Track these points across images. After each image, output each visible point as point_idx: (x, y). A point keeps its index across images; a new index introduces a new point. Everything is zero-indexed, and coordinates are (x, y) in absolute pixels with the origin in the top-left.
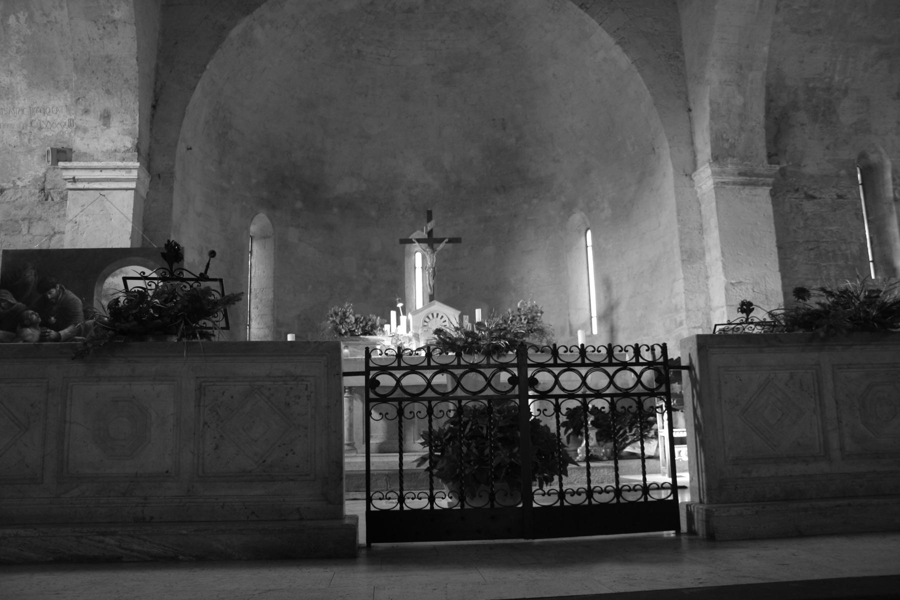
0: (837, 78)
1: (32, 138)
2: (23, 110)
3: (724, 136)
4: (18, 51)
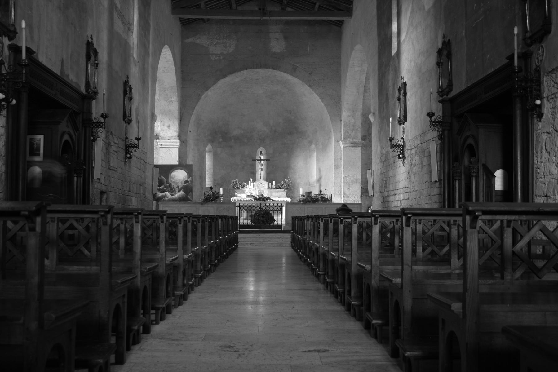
3: (348, 132)
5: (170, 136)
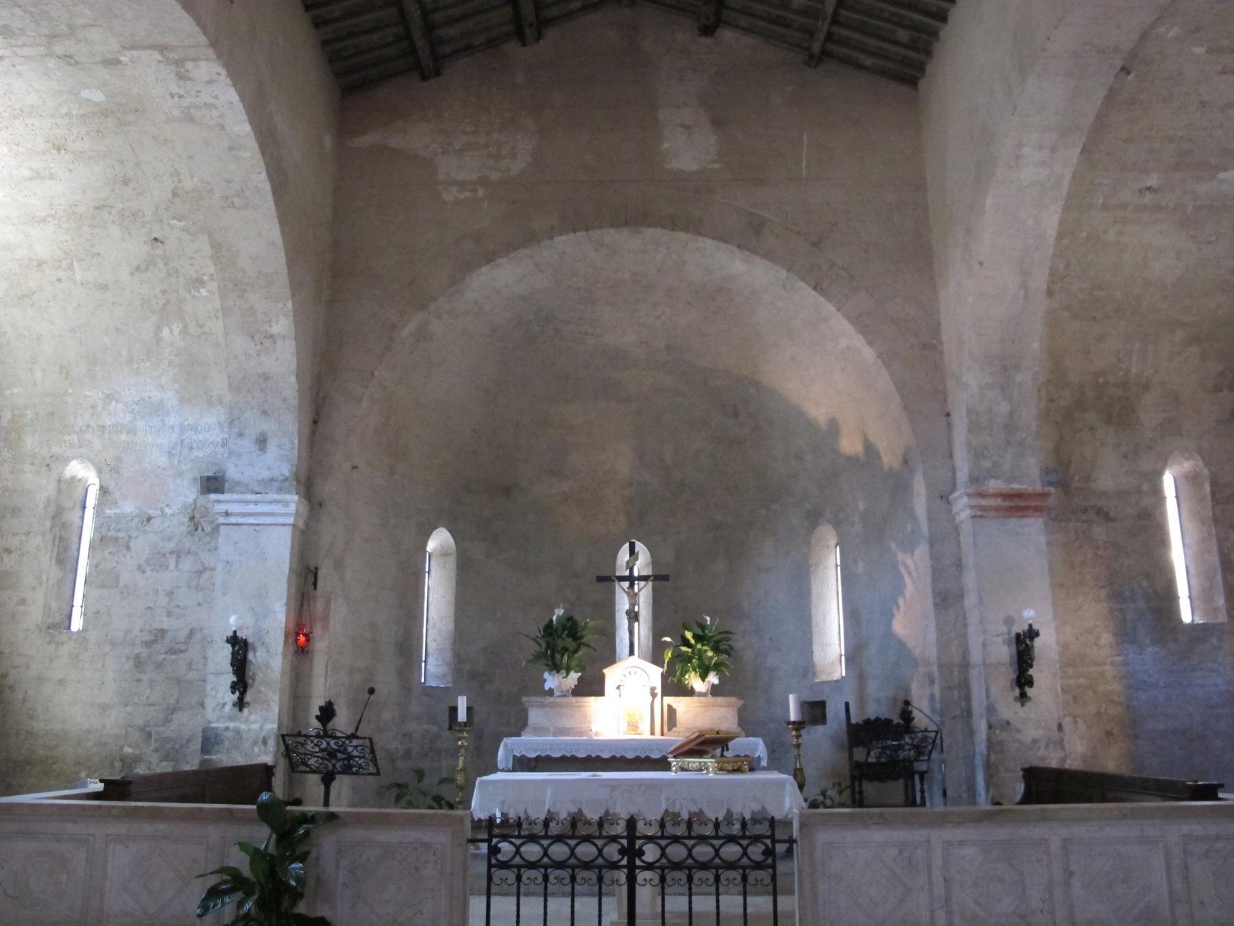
0: (1134, 371)
1: (182, 459)
2: (173, 428)
4: (170, 364)
5: (263, 480)
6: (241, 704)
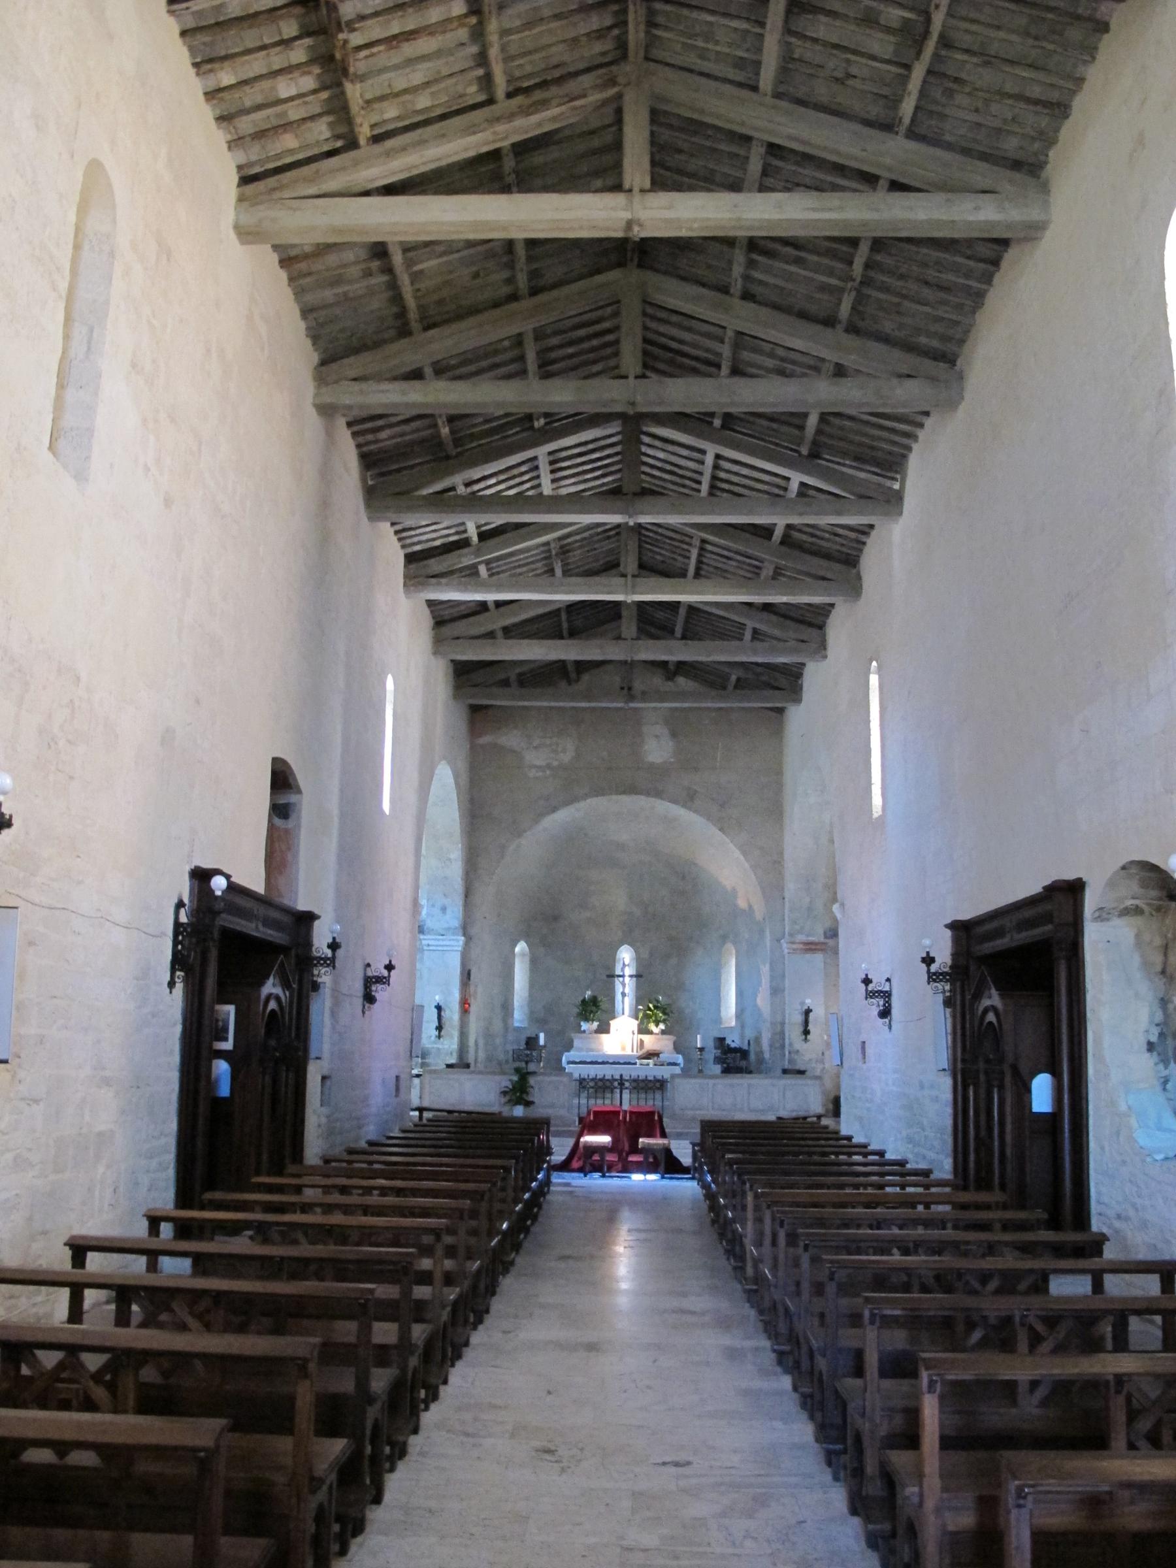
6: (439, 1037)
